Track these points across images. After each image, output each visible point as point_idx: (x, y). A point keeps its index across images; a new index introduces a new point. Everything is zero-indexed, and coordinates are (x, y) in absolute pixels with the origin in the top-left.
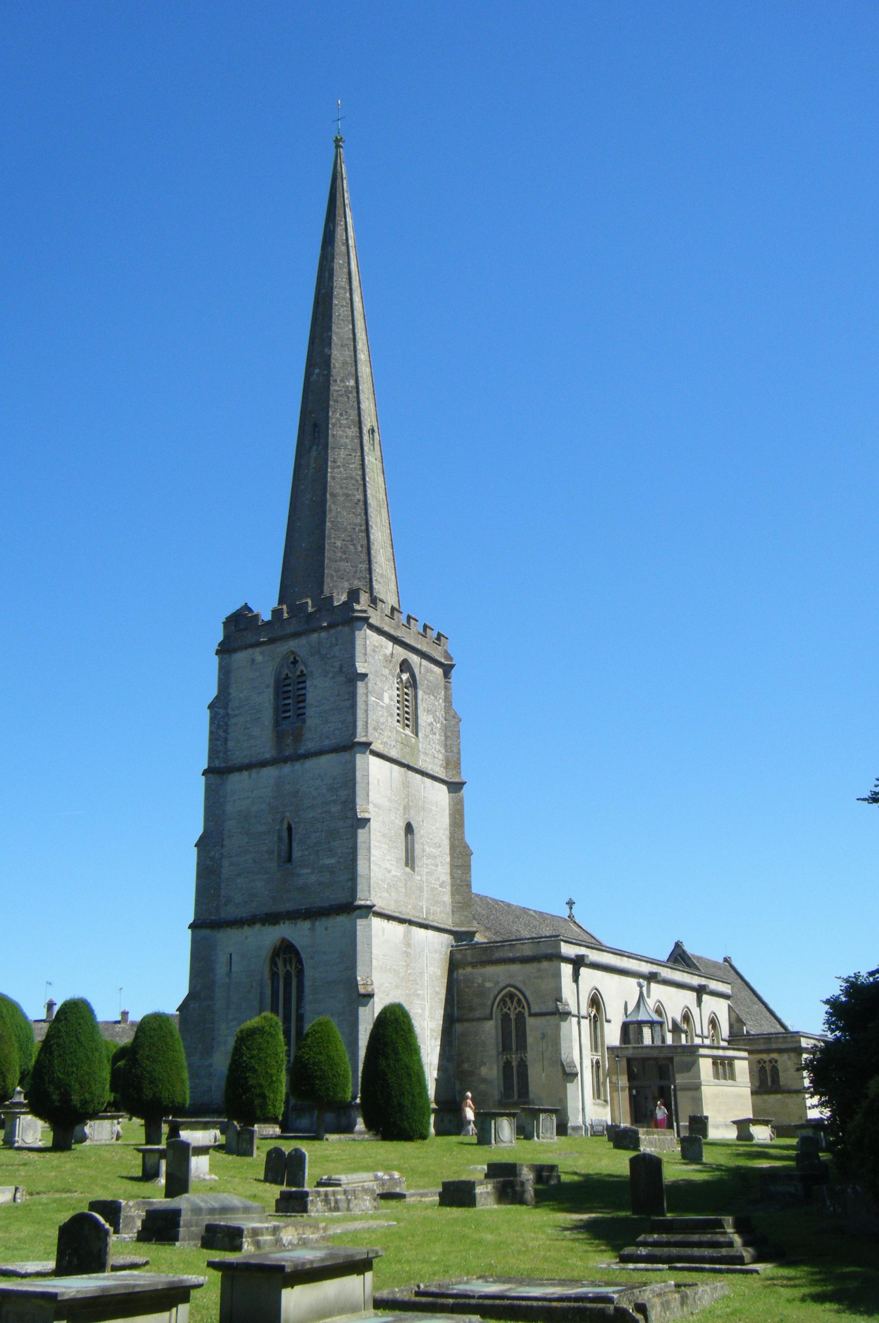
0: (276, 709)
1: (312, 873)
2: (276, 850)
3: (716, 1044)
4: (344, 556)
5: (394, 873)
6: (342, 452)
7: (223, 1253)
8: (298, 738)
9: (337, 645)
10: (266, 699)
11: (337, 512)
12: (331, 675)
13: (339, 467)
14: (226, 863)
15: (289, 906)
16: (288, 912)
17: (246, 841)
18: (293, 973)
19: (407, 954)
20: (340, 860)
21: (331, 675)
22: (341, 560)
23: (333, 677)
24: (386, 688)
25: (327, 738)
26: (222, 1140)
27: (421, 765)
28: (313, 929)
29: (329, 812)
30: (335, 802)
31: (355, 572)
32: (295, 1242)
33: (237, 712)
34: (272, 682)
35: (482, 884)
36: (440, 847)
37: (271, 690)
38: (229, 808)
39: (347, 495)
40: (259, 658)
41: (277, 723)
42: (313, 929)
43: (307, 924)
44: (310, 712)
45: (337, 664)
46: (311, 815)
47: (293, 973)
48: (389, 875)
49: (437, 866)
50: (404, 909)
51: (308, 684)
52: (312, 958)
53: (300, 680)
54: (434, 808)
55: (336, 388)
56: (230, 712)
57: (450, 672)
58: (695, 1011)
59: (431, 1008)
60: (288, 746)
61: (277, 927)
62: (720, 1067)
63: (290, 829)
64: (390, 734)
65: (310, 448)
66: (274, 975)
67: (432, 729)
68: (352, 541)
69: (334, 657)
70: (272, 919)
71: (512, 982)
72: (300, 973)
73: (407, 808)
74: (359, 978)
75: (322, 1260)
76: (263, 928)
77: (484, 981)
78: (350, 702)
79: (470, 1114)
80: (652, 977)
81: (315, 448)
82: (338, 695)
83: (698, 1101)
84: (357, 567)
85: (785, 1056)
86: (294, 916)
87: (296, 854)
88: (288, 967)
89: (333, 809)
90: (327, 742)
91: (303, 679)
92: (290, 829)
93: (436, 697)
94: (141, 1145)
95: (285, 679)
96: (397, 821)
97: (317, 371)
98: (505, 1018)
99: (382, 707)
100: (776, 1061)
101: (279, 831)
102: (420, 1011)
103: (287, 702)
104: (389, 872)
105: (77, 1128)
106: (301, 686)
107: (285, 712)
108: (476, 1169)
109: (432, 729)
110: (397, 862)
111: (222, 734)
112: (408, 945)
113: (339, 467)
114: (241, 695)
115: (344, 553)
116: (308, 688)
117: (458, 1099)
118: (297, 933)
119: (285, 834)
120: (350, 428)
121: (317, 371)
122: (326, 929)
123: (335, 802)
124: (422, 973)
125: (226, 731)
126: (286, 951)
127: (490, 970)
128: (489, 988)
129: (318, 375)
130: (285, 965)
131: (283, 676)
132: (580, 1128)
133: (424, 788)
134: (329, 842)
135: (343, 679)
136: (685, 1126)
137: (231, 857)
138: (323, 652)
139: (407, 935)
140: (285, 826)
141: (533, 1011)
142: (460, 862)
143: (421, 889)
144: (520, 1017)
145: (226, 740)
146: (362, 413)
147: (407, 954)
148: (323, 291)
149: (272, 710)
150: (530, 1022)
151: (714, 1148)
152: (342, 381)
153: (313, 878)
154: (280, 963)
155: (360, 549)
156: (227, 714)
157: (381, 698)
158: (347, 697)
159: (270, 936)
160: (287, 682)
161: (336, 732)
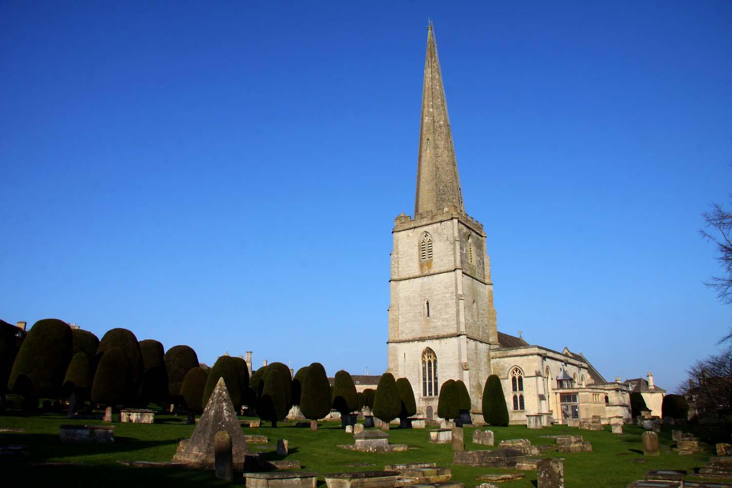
1: (439, 321)
3: (426, 272)
4: (444, 193)
5: (471, 321)
6: (440, 150)
8: (429, 264)
9: (445, 229)
10: (415, 252)
11: (440, 175)
12: (443, 241)
13: (439, 156)
14: (400, 317)
16: (429, 337)
18: (432, 361)
19: (476, 353)
21: (443, 241)
23: (444, 242)
25: (443, 267)
27: (477, 277)
28: (440, 343)
31: (449, 199)
38: (401, 295)
39: (443, 168)
40: (411, 234)
42: (440, 343)
43: (438, 341)
44: (434, 256)
47: (432, 361)
49: (484, 318)
50: (474, 336)
51: (433, 245)
52: (441, 355)
53: (429, 243)
54: (482, 295)
57: (658, 388)
58: (577, 373)
59: (484, 374)
61: (425, 342)
62: (594, 395)
63: (428, 303)
66: (424, 362)
69: (444, 234)
70: (422, 340)
71: (516, 364)
72: (435, 362)
73: (474, 295)
77: (504, 364)
80: (566, 363)
85: (611, 392)
86: (431, 338)
87: (431, 314)
88: (430, 358)
89: (447, 296)
90: (442, 268)
91: (430, 242)
92: (428, 303)
98: (514, 379)
100: (607, 394)
102: (481, 376)
103: (424, 252)
104: (469, 320)
106: (430, 253)
108: (395, 478)
111: (397, 265)
112: (476, 350)
113: (439, 156)
115: (444, 191)
116: (433, 254)
117: (203, 406)
118: (434, 345)
119: (426, 305)
120: (442, 141)
121: (427, 118)
122: (446, 343)
124: (481, 361)
126: (429, 351)
127: (506, 359)
128: (507, 367)
130: (428, 358)
132: (438, 471)
136: (260, 476)
139: (476, 346)
140: (426, 302)
141: (525, 376)
142: (490, 294)
143: (479, 327)
144: (520, 379)
145: (398, 268)
147: (476, 353)
148: (710, 439)
150: (524, 380)
151: (443, 269)
152: (438, 122)
154: (426, 356)
155: (449, 190)
156: (398, 257)
158: (450, 250)
159: (423, 346)
160: (424, 244)
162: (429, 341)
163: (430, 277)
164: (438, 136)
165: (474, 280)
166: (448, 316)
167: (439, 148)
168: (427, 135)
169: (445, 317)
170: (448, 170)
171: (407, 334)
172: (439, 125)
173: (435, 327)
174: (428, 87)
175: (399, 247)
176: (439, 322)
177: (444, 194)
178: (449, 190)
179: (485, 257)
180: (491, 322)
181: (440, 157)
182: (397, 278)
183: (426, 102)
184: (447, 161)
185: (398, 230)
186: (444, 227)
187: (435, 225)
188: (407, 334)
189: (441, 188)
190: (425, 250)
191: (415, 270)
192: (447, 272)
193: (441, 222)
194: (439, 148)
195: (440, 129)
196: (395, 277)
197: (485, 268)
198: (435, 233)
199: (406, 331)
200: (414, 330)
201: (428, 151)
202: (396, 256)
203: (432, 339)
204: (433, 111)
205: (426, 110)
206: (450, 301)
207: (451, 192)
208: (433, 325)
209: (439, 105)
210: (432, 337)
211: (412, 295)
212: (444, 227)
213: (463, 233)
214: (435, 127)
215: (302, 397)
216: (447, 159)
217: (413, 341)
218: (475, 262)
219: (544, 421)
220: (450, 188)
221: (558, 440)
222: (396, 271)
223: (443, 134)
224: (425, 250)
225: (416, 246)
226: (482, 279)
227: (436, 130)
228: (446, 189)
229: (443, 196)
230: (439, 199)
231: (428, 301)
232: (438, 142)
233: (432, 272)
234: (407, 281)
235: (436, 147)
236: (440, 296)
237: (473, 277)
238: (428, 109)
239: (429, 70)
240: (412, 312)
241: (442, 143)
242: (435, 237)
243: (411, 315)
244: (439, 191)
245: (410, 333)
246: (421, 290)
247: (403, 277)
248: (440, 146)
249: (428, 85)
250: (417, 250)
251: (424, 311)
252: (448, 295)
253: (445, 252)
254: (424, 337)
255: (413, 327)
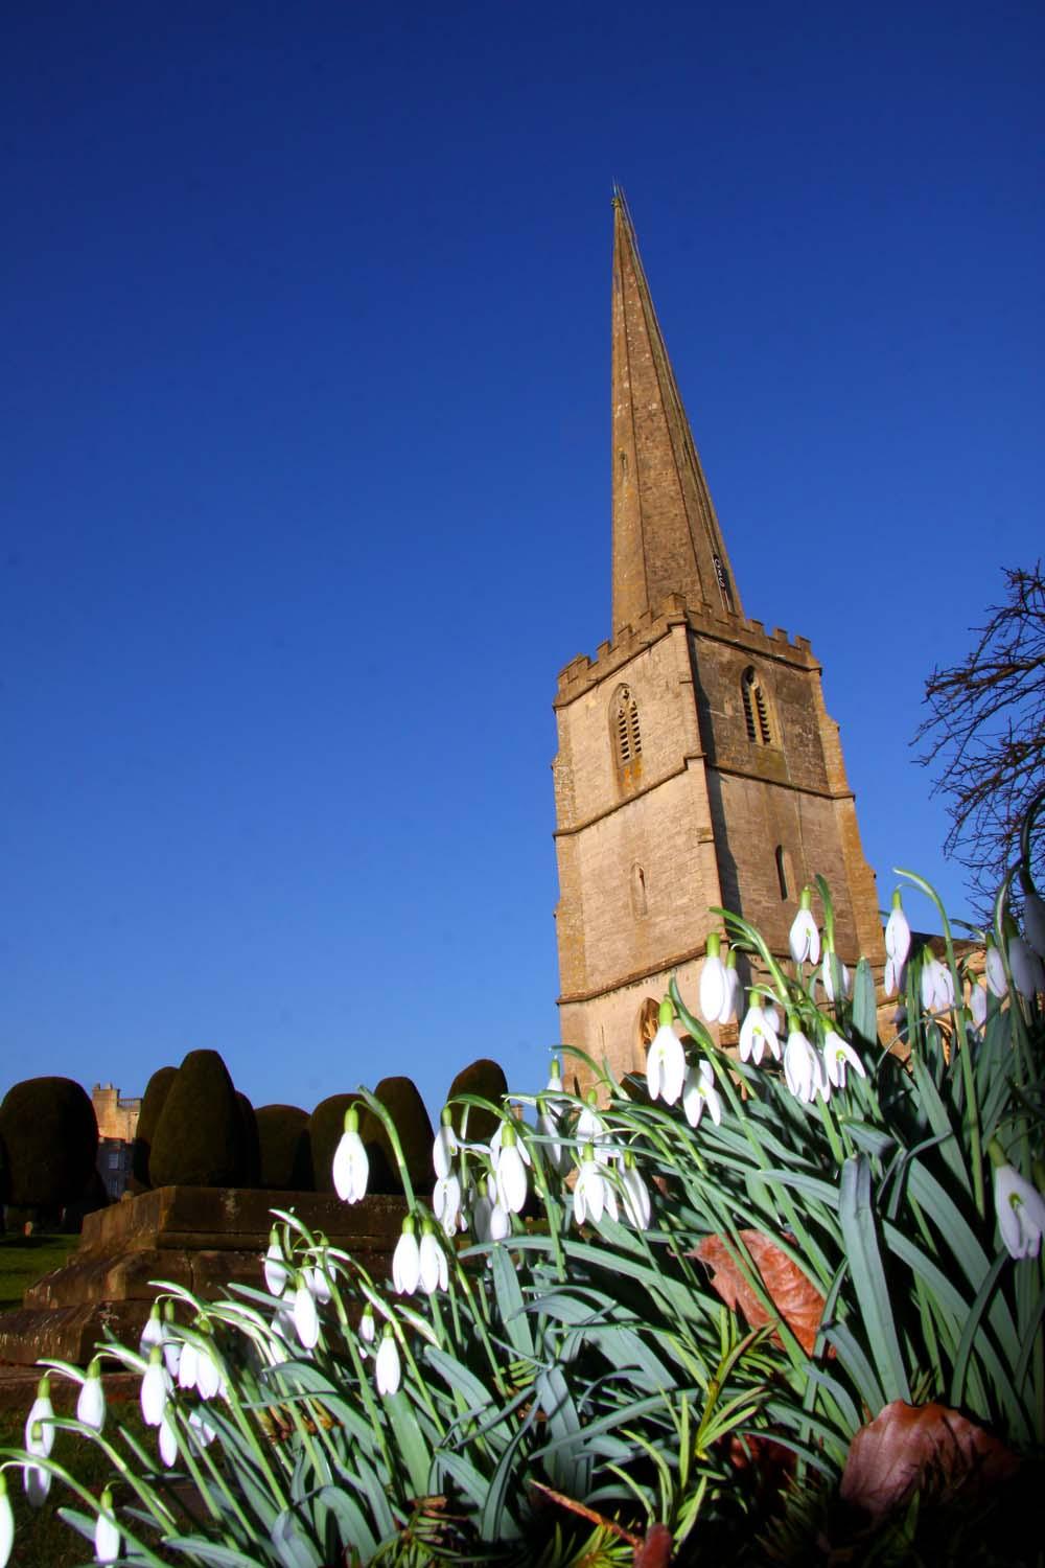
0: (614, 750)
2: (630, 903)
5: (765, 904)
6: (652, 473)
7: (792, 877)
10: (603, 743)
13: (650, 488)
14: (587, 929)
15: (650, 963)
17: (602, 900)
20: (693, 897)
21: (658, 696)
22: (664, 578)
23: (662, 697)
24: (727, 698)
25: (664, 765)
26: (464, 1229)
29: (675, 846)
30: (679, 833)
32: (610, 964)
33: (580, 765)
34: (606, 723)
35: (487, 1485)
36: (831, 871)
37: (607, 732)
41: (617, 766)
45: (663, 682)
46: (658, 855)
48: (757, 907)
54: (816, 828)
55: (639, 415)
56: (574, 768)
60: (629, 786)
64: (739, 748)
65: (622, 479)
67: (801, 741)
68: (672, 557)
70: (634, 981)
74: (714, 731)
75: (575, 940)
76: (627, 992)
78: (681, 718)
79: (1040, 1003)
81: (625, 478)
82: (668, 716)
83: (573, 1206)
84: (681, 581)
86: (653, 973)
90: (664, 770)
93: (802, 706)
94: (507, 1204)
95: (621, 717)
96: (762, 845)
97: (619, 407)
99: (724, 719)
101: (631, 881)
103: (626, 754)
104: (759, 903)
105: (964, 1122)
107: (623, 737)
109: (801, 741)
110: (768, 891)
113: (650, 488)
114: (582, 748)
115: (666, 570)
123: (679, 833)
125: (572, 789)
129: (621, 411)
131: (618, 713)
133: (799, 806)
134: (679, 880)
135: (670, 696)
137: (591, 921)
138: (649, 674)
140: (638, 874)
145: (573, 797)
146: (655, 790)
149: (610, 754)
152: (645, 407)
153: (669, 925)
156: (572, 771)
157: (722, 710)
161: (672, 756)
162: (649, 980)
163: (639, 802)
164: (647, 439)
165: (775, 789)
166: (685, 900)
167: (650, 467)
168: (621, 445)
169: (679, 903)
170: (676, 515)
171: (602, 973)
172: (646, 414)
173: (659, 940)
174: (619, 337)
175: (572, 745)
176: (668, 923)
177: (669, 578)
178: (682, 562)
179: (822, 725)
180: (860, 903)
181: (654, 490)
182: (573, 825)
183: (615, 372)
184: (672, 493)
185: (563, 702)
186: (657, 659)
187: (639, 660)
188: (602, 973)
189: (658, 564)
190: (625, 732)
191: (605, 791)
192: (673, 776)
193: (650, 645)
194: (650, 467)
195: (649, 422)
196: (565, 825)
197: (827, 753)
198: (639, 681)
199: (602, 966)
200: (617, 957)
201: (625, 484)
202: (565, 769)
203: (656, 973)
204: (636, 386)
205: (616, 389)
206: (688, 856)
207: (687, 568)
208: (657, 932)
209: (647, 367)
210: (655, 967)
211: (606, 862)
212: (657, 659)
213: (721, 663)
214: (638, 421)
215: (5, 1216)
216: (673, 488)
217: (614, 989)
218: (780, 741)
219: (824, 1193)
220: (685, 560)
221: (791, 1280)
222: (567, 808)
223: (657, 434)
224: (625, 732)
225: (604, 729)
226: (816, 786)
227: (641, 427)
228: (673, 564)
229: (665, 582)
230: (653, 592)
231: (641, 871)
232: (645, 455)
233: (642, 788)
234: (593, 828)
235: (641, 468)
236: (665, 848)
237: (768, 782)
238: (621, 385)
239: (620, 296)
240: (608, 908)
241: (658, 453)
242: (639, 690)
243: (607, 917)
244: (655, 573)
245: (610, 967)
246: (624, 841)
247: (586, 819)
248: (652, 463)
249: (619, 330)
250: (608, 739)
251: (633, 899)
252: (680, 840)
253: (666, 723)
254: (638, 974)
255: (614, 951)
